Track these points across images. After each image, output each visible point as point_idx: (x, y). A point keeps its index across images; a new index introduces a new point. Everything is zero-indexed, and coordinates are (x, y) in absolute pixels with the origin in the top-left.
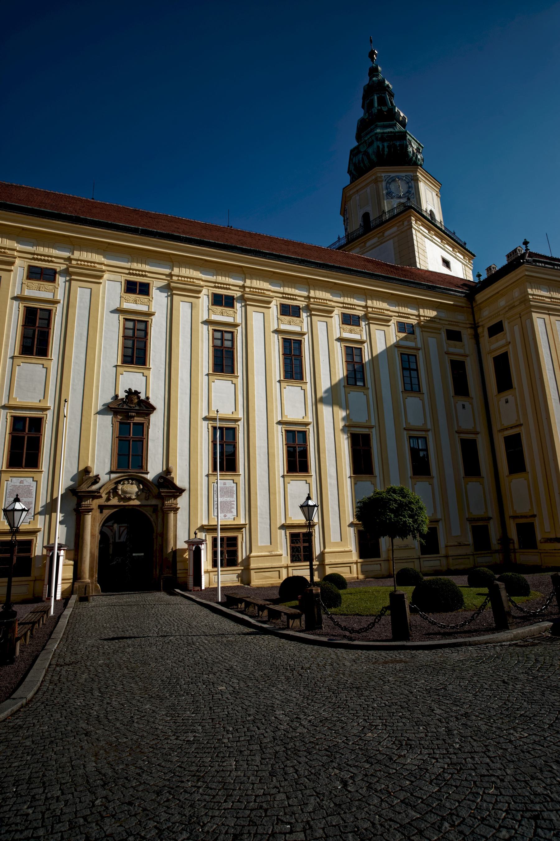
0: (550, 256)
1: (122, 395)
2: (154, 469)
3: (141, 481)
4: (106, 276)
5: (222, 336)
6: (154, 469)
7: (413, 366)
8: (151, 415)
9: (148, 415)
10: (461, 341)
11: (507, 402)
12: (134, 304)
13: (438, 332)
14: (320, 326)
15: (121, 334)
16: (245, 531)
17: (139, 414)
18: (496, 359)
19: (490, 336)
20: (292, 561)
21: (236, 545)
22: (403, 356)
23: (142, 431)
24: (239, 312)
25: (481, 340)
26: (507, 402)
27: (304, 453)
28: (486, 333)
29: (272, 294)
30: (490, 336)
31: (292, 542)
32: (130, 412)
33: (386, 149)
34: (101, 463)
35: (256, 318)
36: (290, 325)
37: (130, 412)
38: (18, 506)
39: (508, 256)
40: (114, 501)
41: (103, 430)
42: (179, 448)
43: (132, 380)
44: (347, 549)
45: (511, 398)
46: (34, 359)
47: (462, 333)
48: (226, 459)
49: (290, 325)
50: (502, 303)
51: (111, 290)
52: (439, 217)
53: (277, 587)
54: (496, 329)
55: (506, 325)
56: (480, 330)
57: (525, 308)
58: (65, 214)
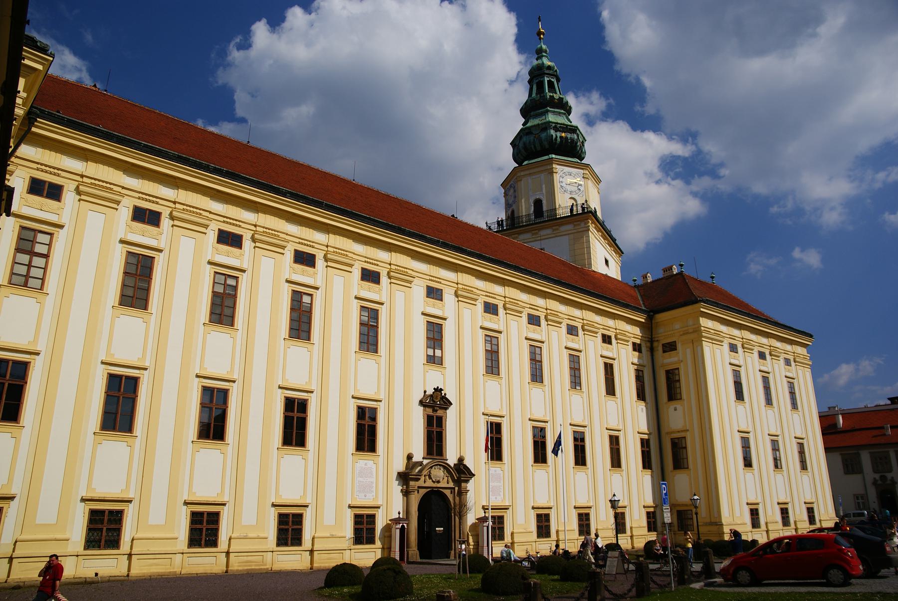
0: (695, 277)
1: (430, 391)
2: (452, 459)
3: (446, 467)
4: (416, 281)
5: (35, 237)
6: (452, 459)
7: (538, 358)
8: (448, 411)
9: (446, 409)
10: (241, 248)
11: (675, 410)
12: (434, 308)
13: (115, 206)
14: (399, 294)
15: (122, 271)
16: (509, 512)
17: (441, 408)
18: (668, 372)
19: (664, 352)
20: (278, 545)
21: (503, 523)
22: (217, 276)
23: (440, 421)
24: (501, 319)
25: (656, 353)
26: (675, 410)
27: (373, 431)
28: (660, 349)
29: (355, 257)
30: (664, 352)
31: (356, 523)
32: (436, 404)
33: (559, 139)
34: (419, 455)
35: (95, 220)
36: (143, 235)
37: (436, 404)
38: (696, 497)
39: (665, 270)
40: (429, 483)
41: (418, 416)
42: (464, 441)
43: (433, 379)
44: (262, 535)
45: (678, 407)
46: (369, 355)
47: (65, 189)
48: (495, 449)
49: (491, 322)
50: (677, 326)
51: (419, 290)
52: (599, 214)
53: (33, 586)
54: (670, 347)
55: (679, 346)
56: (655, 344)
57: (696, 336)
58: (21, 87)
